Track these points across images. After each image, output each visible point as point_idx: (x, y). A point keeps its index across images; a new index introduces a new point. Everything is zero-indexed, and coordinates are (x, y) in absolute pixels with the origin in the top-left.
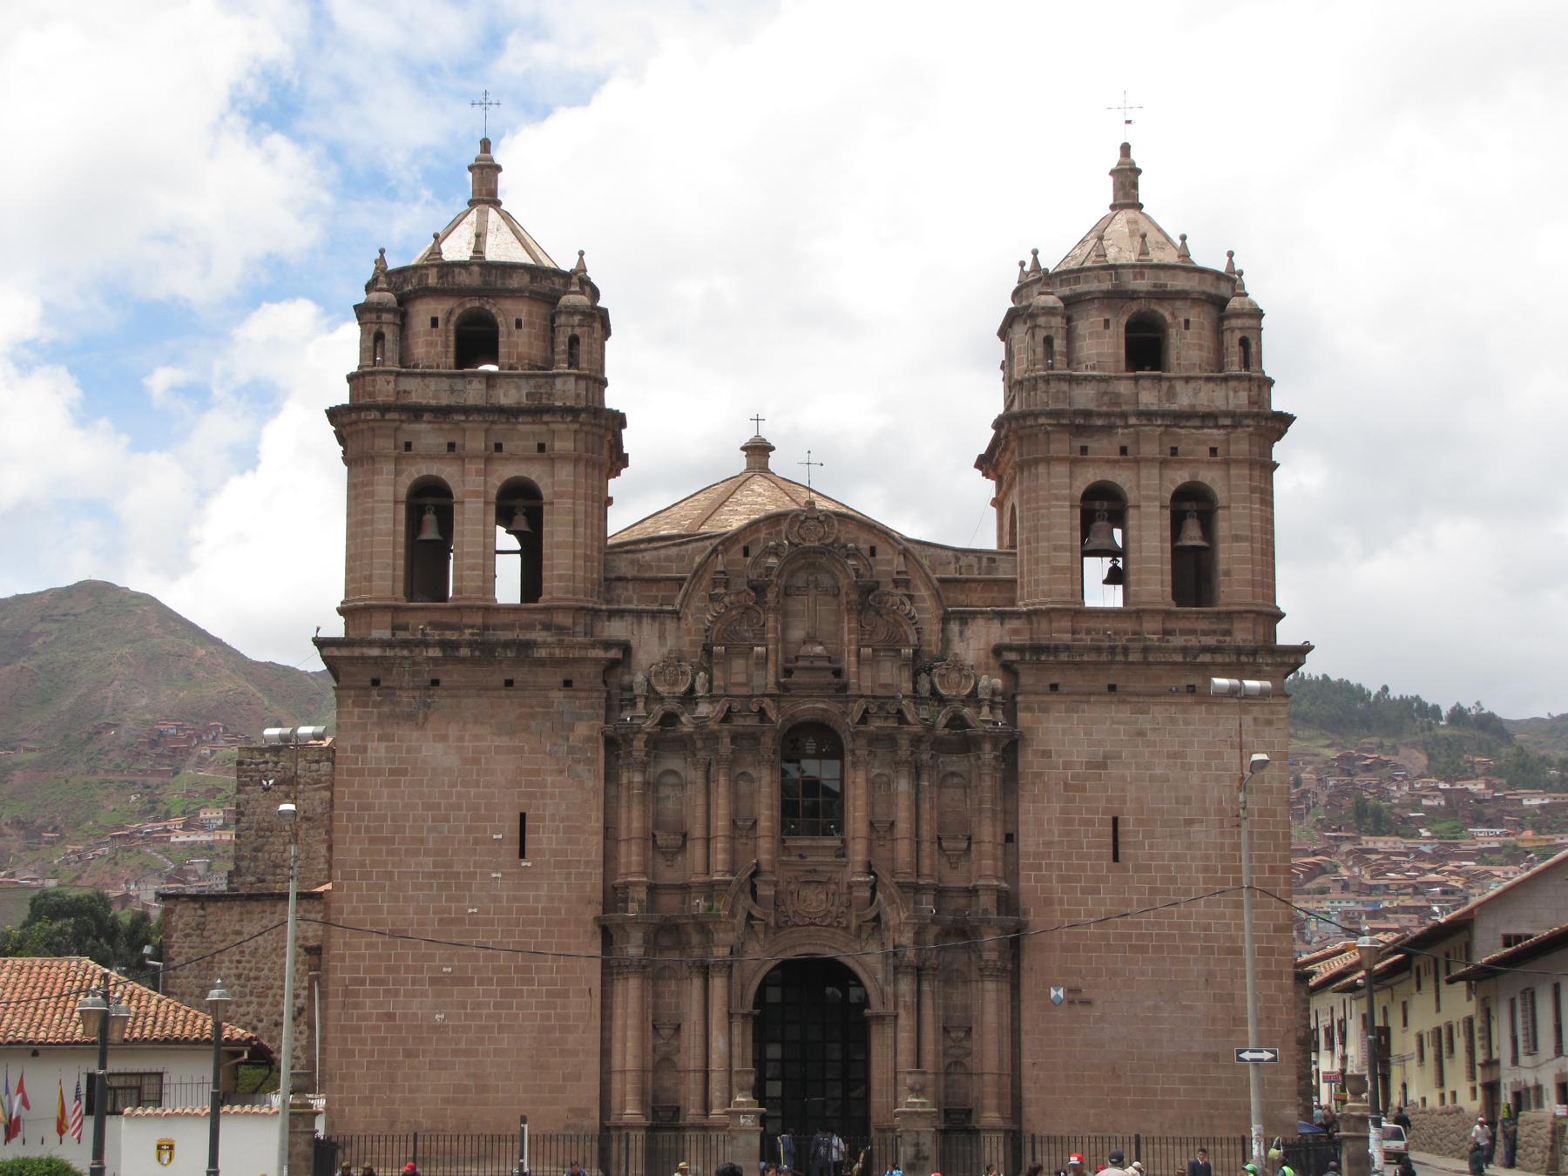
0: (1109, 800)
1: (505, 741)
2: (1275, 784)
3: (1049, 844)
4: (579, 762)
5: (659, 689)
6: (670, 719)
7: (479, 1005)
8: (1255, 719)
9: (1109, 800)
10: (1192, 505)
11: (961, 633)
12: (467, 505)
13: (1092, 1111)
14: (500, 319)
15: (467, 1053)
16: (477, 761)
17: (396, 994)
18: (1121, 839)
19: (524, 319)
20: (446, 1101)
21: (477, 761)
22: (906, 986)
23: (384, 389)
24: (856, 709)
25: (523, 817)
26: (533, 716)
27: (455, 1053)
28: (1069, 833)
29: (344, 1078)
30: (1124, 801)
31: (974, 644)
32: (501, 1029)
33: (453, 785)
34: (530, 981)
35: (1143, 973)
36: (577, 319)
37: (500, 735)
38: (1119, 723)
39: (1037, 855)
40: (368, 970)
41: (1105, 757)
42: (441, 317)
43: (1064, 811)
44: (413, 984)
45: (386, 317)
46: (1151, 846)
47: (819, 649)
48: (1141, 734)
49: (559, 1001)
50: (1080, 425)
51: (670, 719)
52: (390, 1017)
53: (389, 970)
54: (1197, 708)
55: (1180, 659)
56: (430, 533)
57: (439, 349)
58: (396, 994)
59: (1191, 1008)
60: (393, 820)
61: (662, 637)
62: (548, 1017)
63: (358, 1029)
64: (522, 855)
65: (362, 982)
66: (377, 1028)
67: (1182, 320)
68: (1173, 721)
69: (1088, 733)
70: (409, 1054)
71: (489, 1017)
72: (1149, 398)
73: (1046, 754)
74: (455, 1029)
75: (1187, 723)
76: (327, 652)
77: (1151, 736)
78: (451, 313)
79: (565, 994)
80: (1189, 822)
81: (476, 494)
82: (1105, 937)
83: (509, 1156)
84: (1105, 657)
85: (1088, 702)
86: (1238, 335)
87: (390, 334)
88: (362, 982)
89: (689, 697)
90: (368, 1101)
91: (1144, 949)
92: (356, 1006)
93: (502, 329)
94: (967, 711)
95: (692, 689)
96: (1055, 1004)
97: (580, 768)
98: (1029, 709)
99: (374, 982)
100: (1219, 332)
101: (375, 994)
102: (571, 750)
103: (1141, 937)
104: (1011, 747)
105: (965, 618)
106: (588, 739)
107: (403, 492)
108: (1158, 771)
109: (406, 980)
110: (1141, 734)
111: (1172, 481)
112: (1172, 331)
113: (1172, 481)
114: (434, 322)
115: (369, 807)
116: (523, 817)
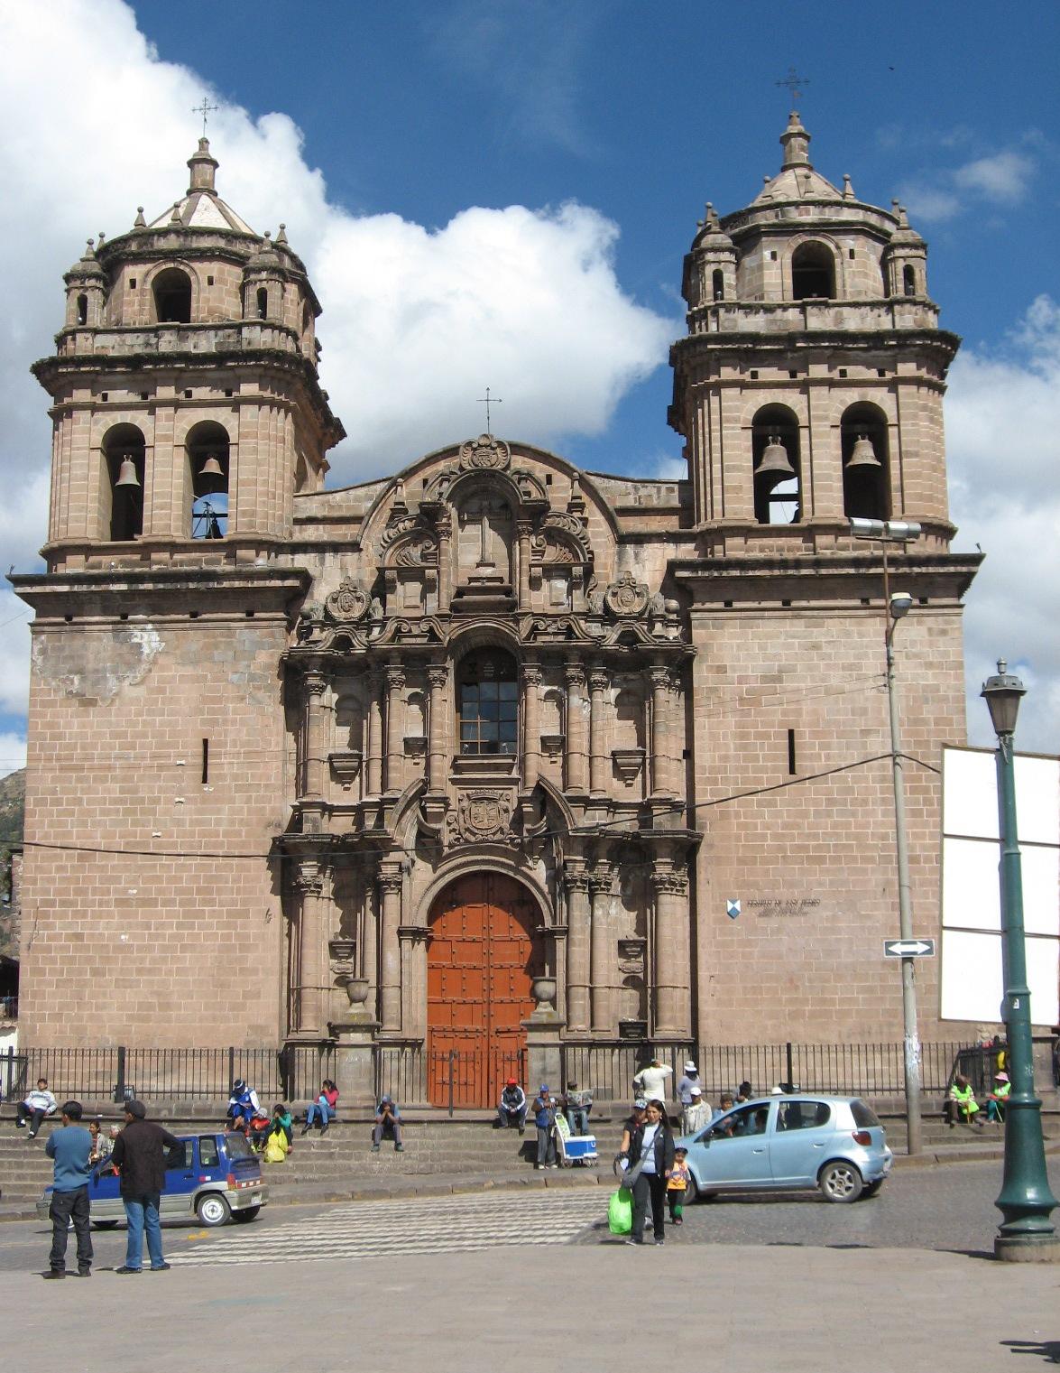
0: (784, 713)
1: (189, 671)
2: (951, 694)
3: (725, 758)
4: (259, 688)
5: (335, 614)
6: (343, 643)
7: (162, 926)
8: (930, 630)
9: (784, 713)
10: (862, 423)
11: (636, 555)
12: (157, 449)
13: (770, 1023)
14: (193, 278)
15: (150, 971)
16: (161, 691)
17: (84, 915)
18: (797, 752)
19: (215, 275)
20: (131, 1018)
21: (161, 691)
22: (579, 898)
23: (84, 345)
24: (525, 626)
25: (205, 742)
26: (216, 646)
27: (140, 971)
28: (744, 747)
29: (35, 995)
30: (798, 712)
31: (650, 565)
32: (184, 948)
33: (139, 714)
34: (211, 902)
35: (821, 884)
36: (264, 275)
37: (184, 665)
38: (794, 637)
39: (712, 769)
40: (58, 892)
41: (780, 671)
42: (138, 278)
43: (738, 725)
44: (100, 905)
45: (92, 282)
46: (828, 757)
47: (488, 572)
48: (816, 647)
49: (239, 921)
50: (749, 351)
51: (343, 643)
52: (79, 937)
53: (79, 892)
54: (871, 621)
55: (852, 571)
56: (129, 478)
57: (136, 307)
58: (84, 915)
59: (868, 917)
60: (83, 748)
61: (343, 568)
62: (228, 937)
63: (48, 949)
64: (205, 780)
65: (52, 903)
66: (66, 948)
67: (846, 251)
68: (848, 634)
69: (762, 648)
70: (96, 972)
71: (172, 937)
72: (819, 321)
73: (721, 669)
74: (140, 949)
75: (861, 635)
76: (20, 590)
77: (826, 650)
78: (147, 275)
79: (245, 914)
80: (865, 733)
81: (167, 438)
82: (781, 848)
83: (190, 1072)
84: (776, 572)
85: (762, 618)
86: (901, 264)
87: (94, 298)
88: (52, 903)
89: (366, 622)
90: (58, 1017)
91: (821, 860)
92: (48, 926)
93: (194, 286)
94: (641, 628)
95: (367, 615)
96: (733, 914)
97: (260, 694)
98: (704, 627)
99: (64, 903)
100: (885, 264)
101: (63, 915)
102: (252, 678)
103: (818, 847)
104: (681, 665)
105: (640, 539)
106: (268, 667)
107: (98, 440)
108: (834, 682)
109: (94, 901)
110: (816, 647)
111: (842, 402)
112: (837, 261)
113: (842, 402)
114: (133, 283)
115: (60, 736)
116: (205, 742)
